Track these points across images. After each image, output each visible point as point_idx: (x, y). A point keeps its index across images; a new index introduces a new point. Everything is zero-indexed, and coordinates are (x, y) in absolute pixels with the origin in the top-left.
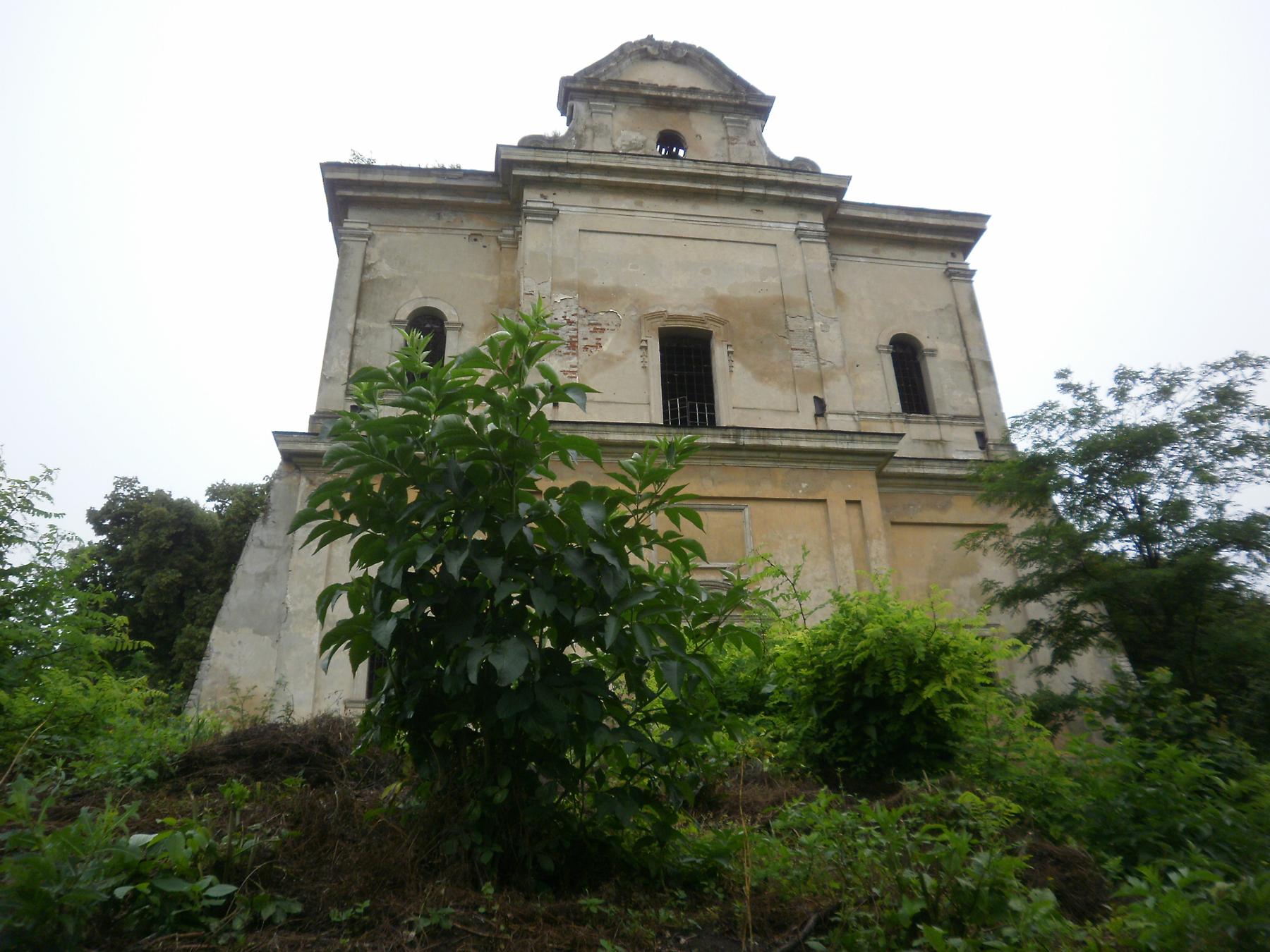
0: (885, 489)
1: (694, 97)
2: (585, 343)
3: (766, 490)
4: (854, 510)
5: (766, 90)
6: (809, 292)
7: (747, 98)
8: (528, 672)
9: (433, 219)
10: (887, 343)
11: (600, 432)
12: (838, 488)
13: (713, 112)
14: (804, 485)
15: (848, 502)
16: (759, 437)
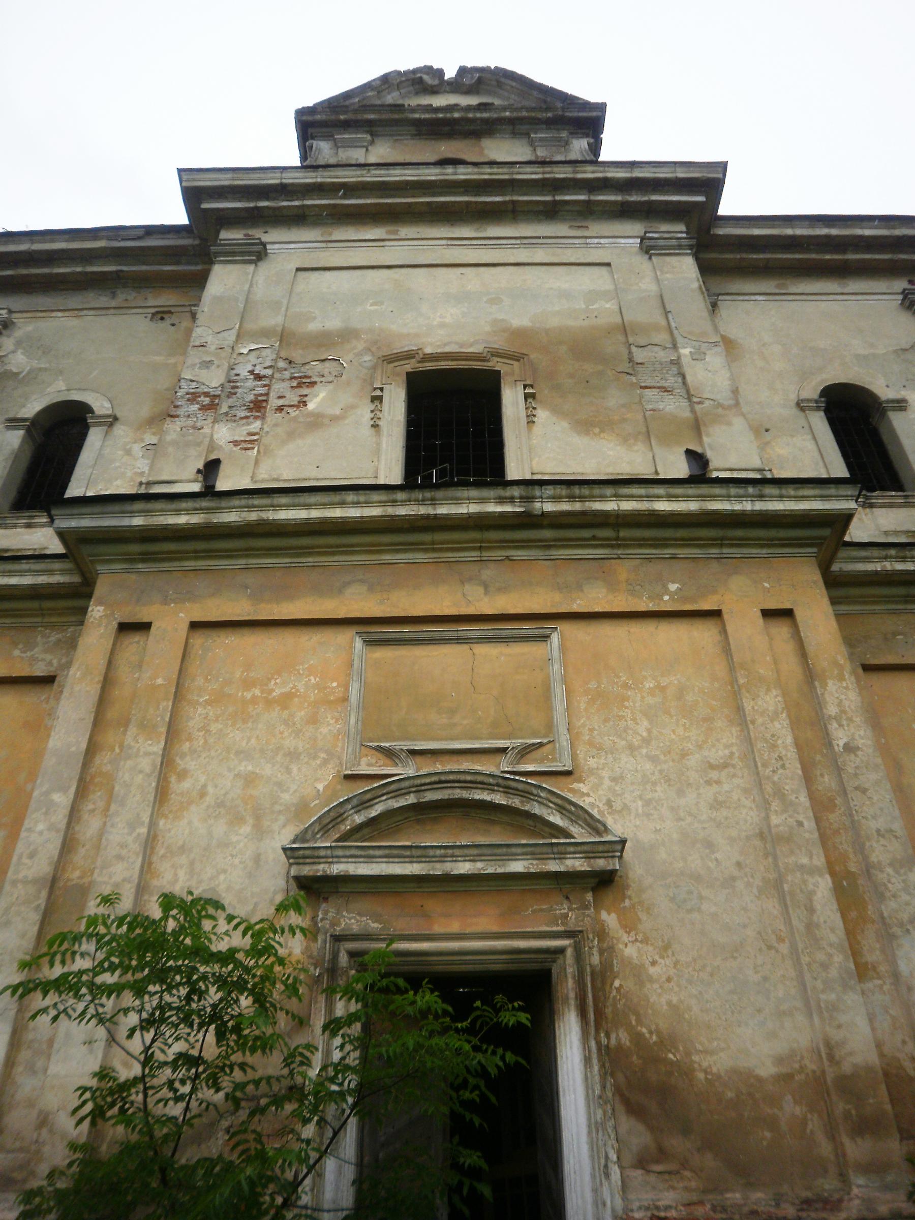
0: (844, 608)
1: (486, 115)
2: (281, 402)
3: (596, 598)
4: (781, 630)
5: (591, 95)
6: (666, 313)
7: (563, 109)
8: (341, 1018)
9: (105, 299)
10: (815, 396)
11: (261, 508)
12: (742, 592)
13: (515, 134)
14: (673, 587)
15: (768, 614)
16: (572, 498)
